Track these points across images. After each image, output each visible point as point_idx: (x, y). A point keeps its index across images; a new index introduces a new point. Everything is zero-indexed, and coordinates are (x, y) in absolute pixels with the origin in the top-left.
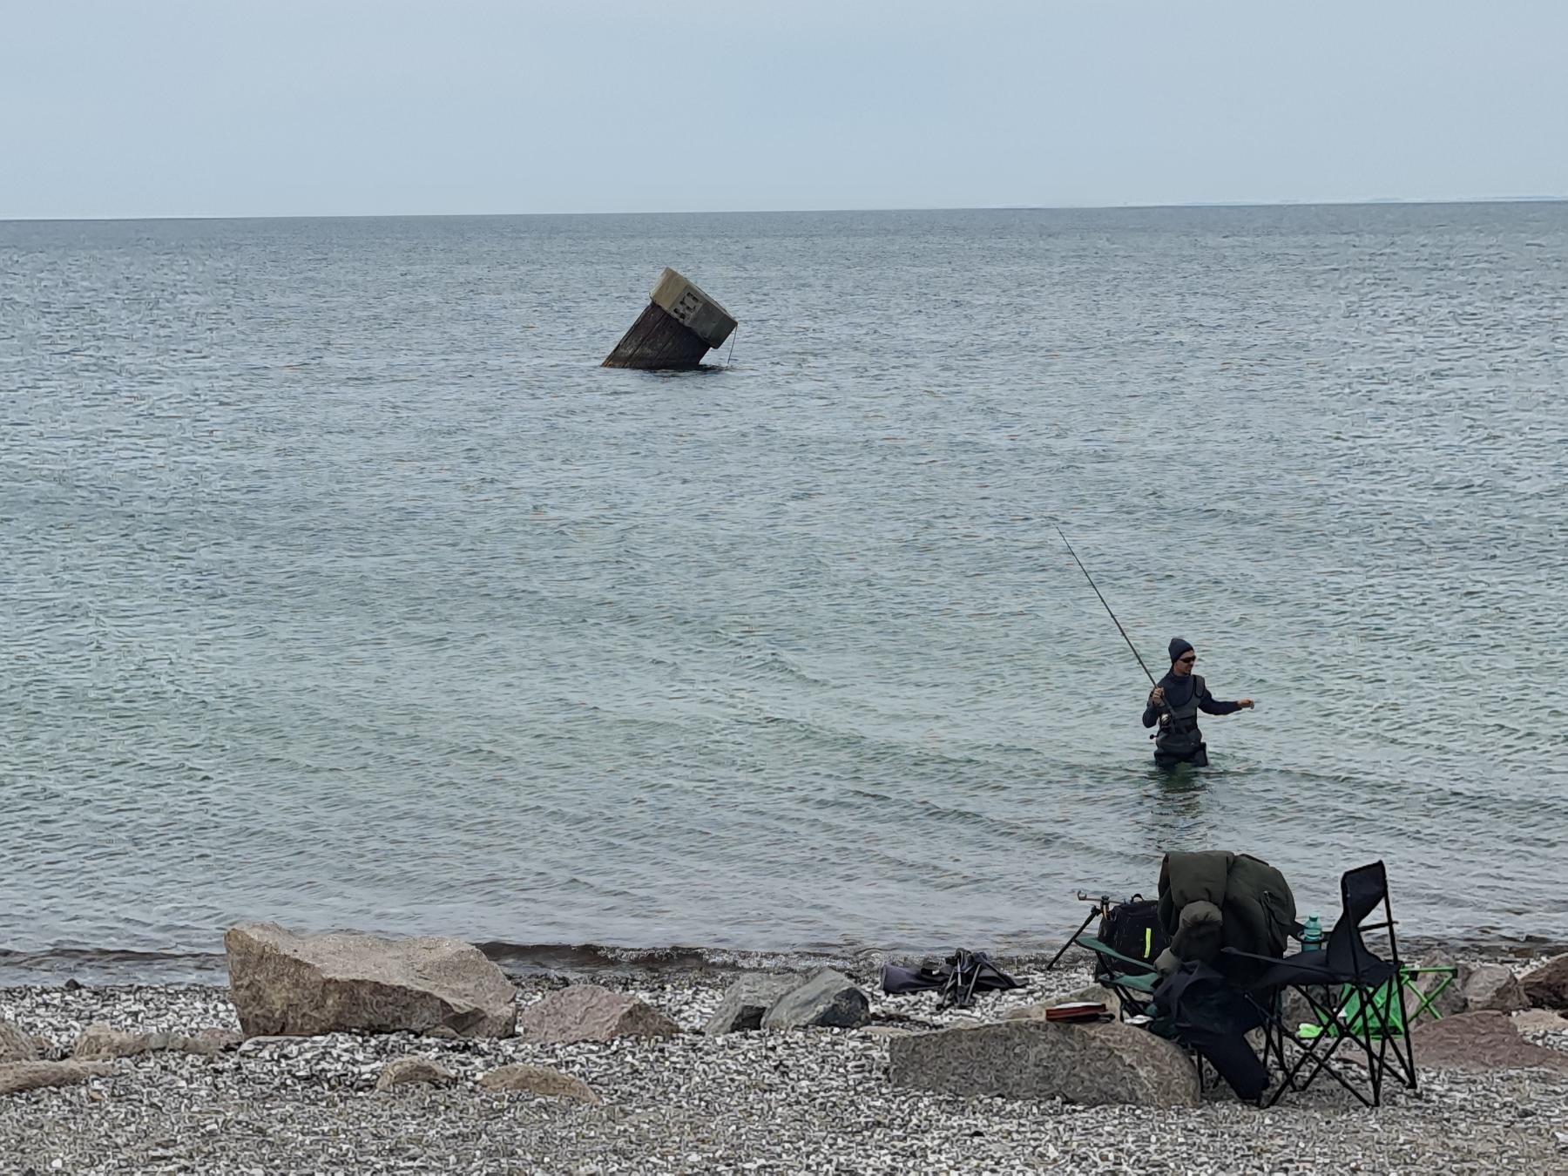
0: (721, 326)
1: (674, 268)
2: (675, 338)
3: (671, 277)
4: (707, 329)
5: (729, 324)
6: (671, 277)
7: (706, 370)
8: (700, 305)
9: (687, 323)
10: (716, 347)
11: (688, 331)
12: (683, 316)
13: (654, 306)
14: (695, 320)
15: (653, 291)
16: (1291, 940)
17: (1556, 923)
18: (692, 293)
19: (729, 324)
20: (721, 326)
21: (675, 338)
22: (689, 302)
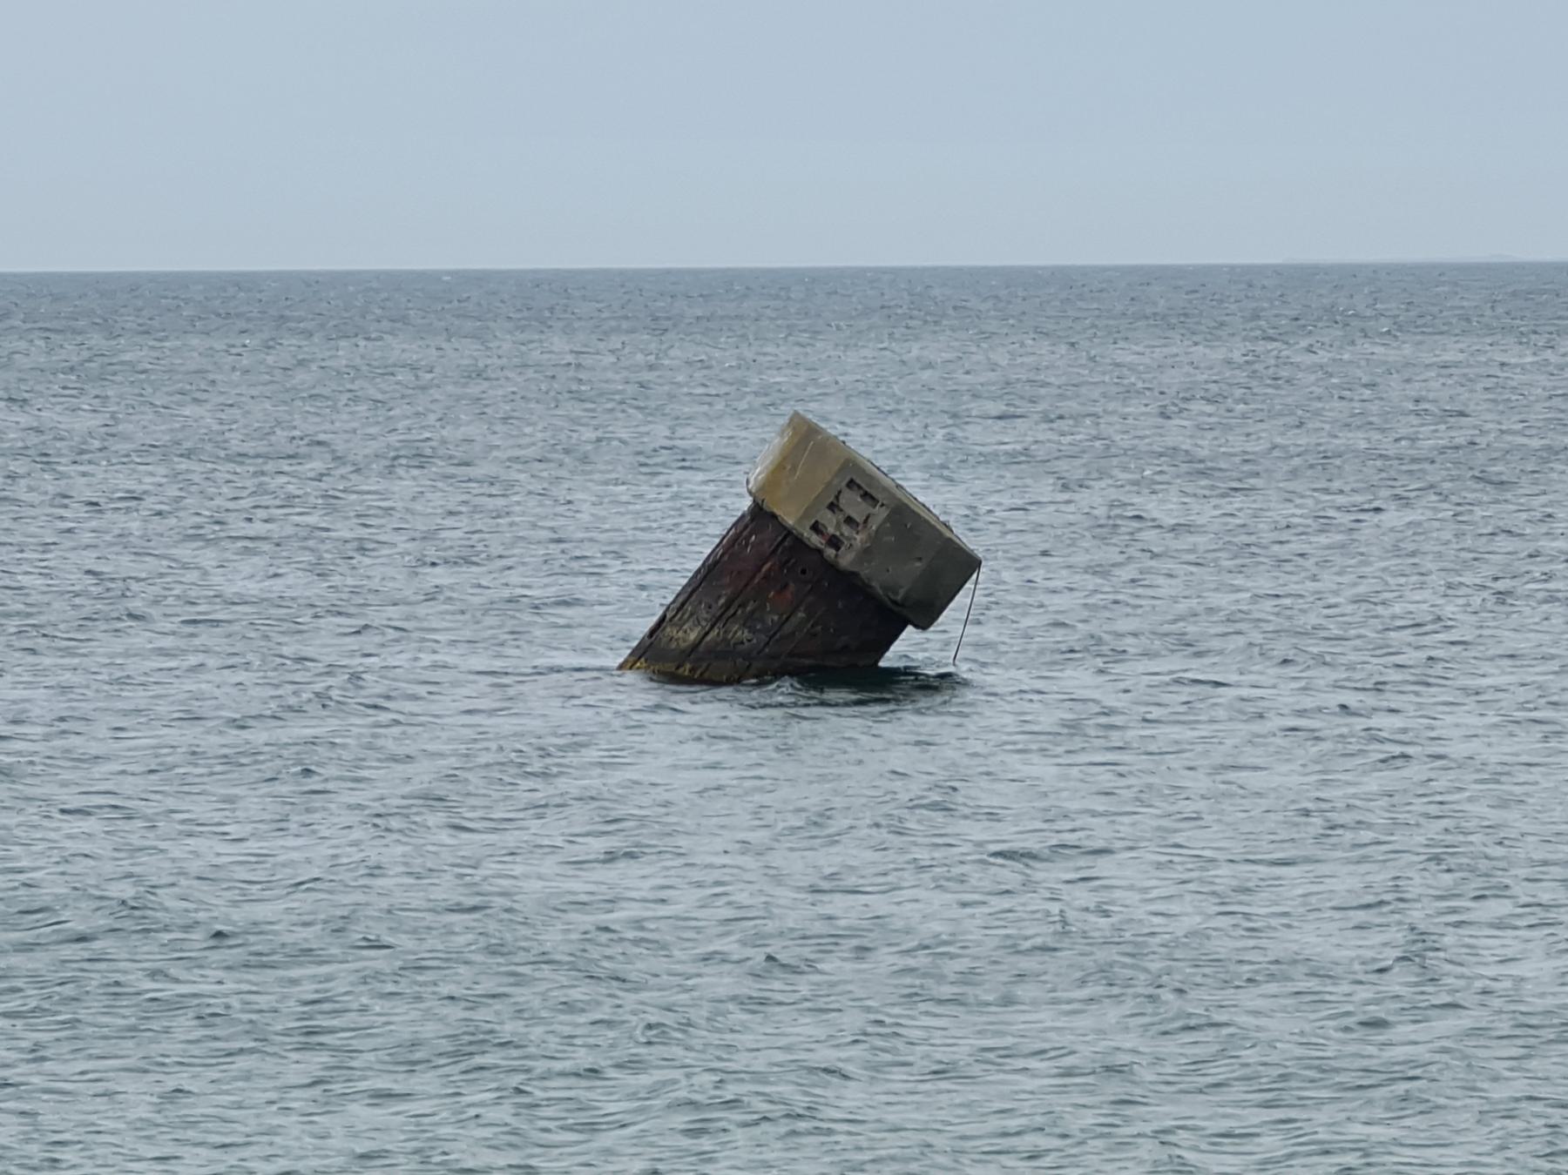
0: (936, 570)
1: (812, 411)
2: (817, 604)
3: (806, 440)
4: (895, 577)
5: (952, 566)
6: (806, 440)
7: (893, 677)
8: (880, 514)
9: (846, 560)
10: (923, 625)
11: (848, 583)
12: (834, 542)
13: (759, 515)
14: (866, 553)
15: (757, 474)
16: (886, 539)
17: (1537, 669)
18: (858, 481)
19: (952, 566)
20: (936, 570)
21: (817, 604)
22: (853, 505)
